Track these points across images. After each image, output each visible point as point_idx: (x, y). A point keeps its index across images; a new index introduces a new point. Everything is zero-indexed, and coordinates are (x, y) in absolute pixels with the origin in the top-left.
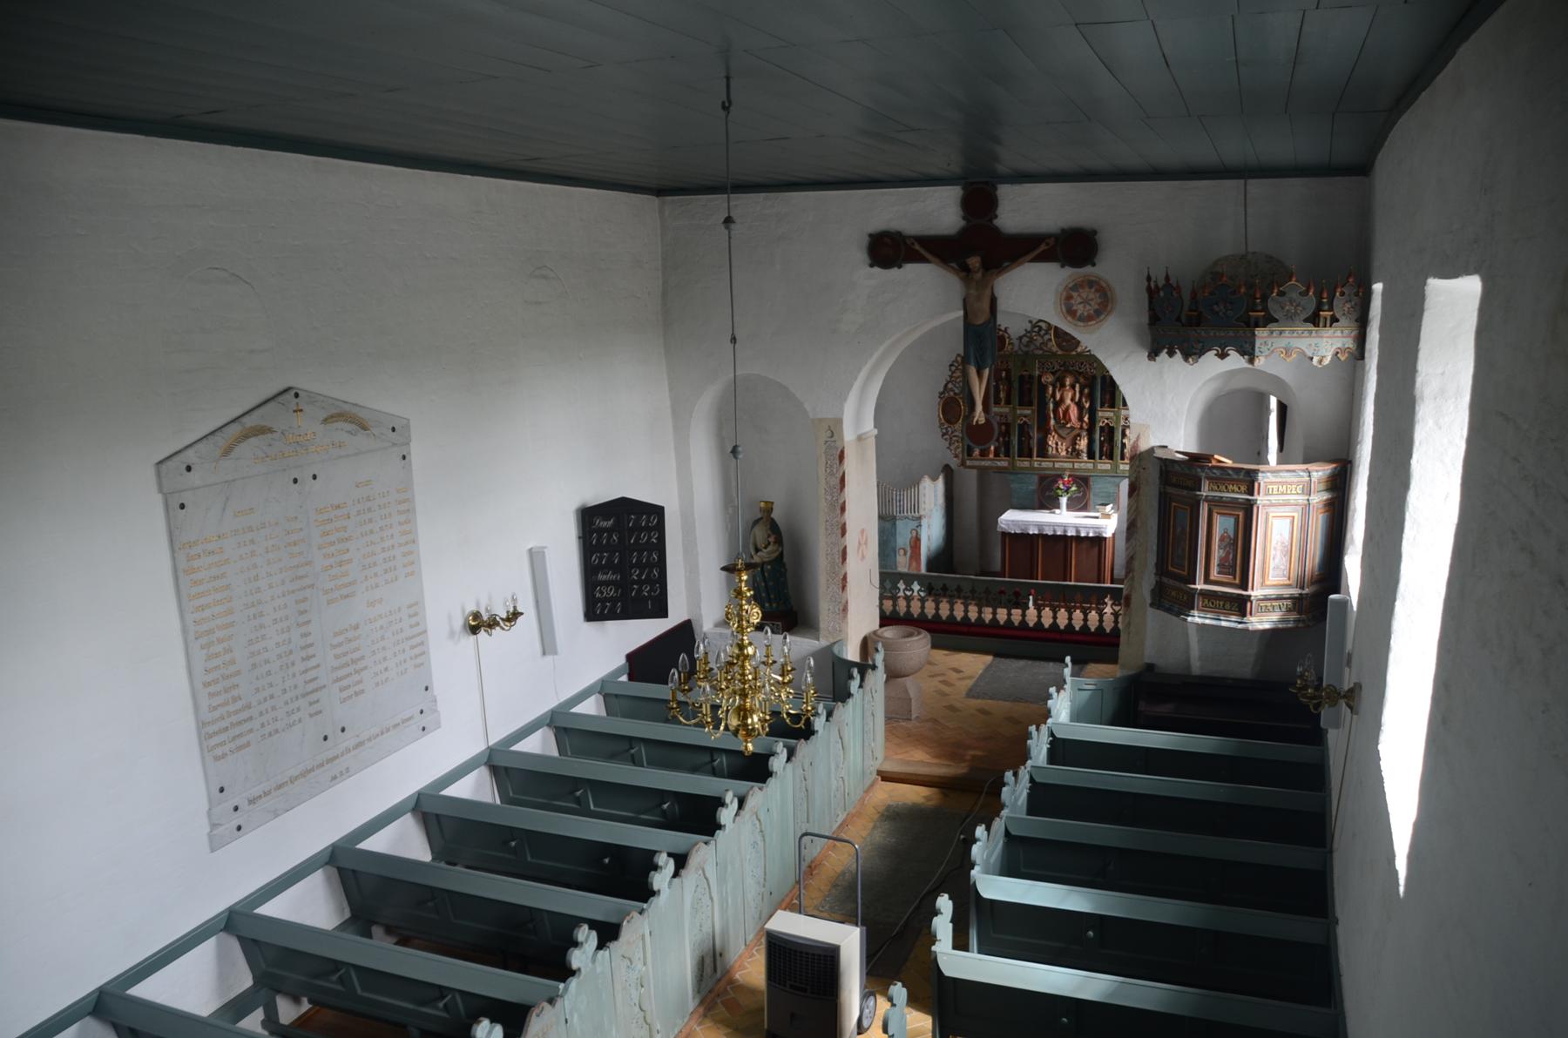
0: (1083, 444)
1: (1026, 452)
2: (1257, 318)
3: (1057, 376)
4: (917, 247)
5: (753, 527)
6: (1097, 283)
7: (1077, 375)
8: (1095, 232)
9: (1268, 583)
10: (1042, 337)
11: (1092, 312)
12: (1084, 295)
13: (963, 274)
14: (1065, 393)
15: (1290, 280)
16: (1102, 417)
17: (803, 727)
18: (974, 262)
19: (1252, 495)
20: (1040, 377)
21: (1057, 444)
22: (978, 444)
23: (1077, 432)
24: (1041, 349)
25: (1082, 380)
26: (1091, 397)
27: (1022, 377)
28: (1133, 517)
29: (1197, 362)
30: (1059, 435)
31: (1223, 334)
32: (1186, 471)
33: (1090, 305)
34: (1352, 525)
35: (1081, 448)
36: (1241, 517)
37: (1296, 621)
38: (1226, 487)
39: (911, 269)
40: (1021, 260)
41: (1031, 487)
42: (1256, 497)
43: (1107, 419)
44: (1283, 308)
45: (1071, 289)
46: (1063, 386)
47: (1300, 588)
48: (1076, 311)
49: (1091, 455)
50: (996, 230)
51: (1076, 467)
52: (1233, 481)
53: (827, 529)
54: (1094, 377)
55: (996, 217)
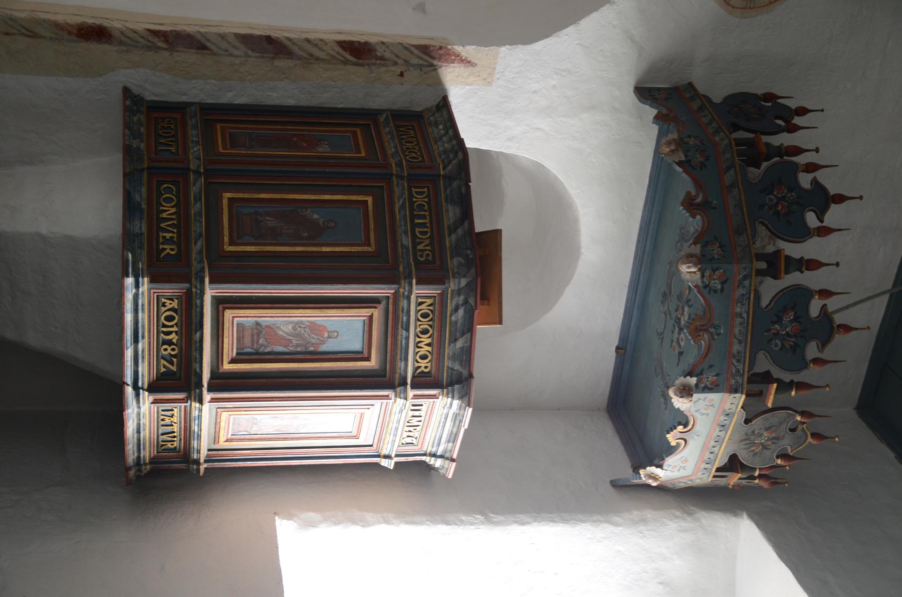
9: (224, 415)
28: (295, 49)
31: (736, 331)
32: (450, 241)
38: (424, 332)
42: (411, 393)
44: (767, 429)
47: (208, 456)
52: (438, 346)
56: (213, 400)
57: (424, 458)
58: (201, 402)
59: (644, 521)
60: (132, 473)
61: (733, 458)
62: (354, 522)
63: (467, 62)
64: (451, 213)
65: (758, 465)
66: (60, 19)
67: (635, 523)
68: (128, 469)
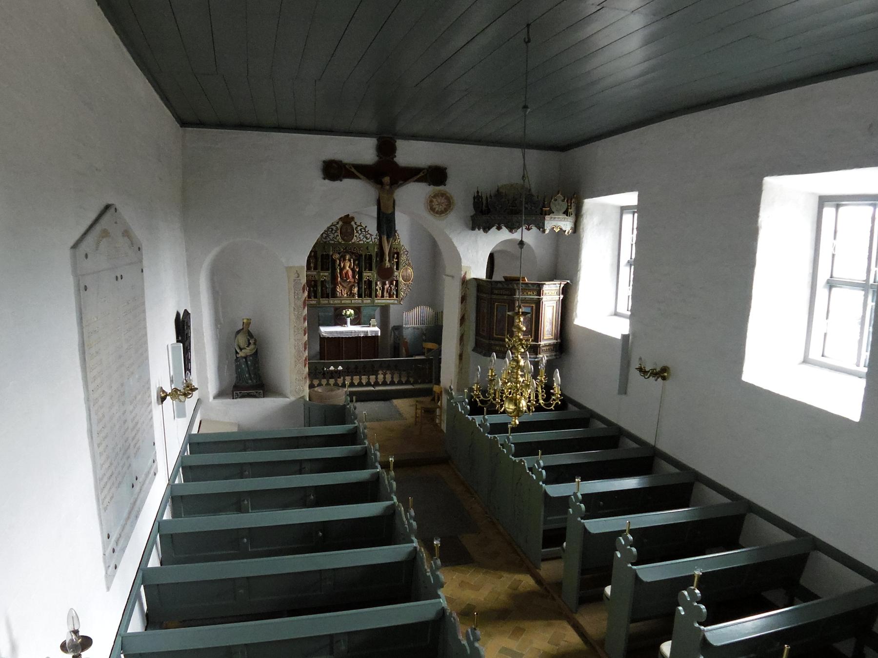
0: (356, 290)
1: (325, 295)
2: (546, 211)
3: (341, 254)
4: (353, 170)
5: (236, 337)
6: (445, 194)
7: (352, 253)
8: (446, 169)
9: (545, 338)
10: (334, 234)
11: (443, 209)
12: (439, 201)
13: (379, 186)
14: (346, 263)
15: (558, 194)
16: (366, 276)
17: (553, 409)
18: (387, 180)
19: (540, 296)
20: (332, 255)
21: (341, 291)
22: (387, 278)
23: (353, 284)
24: (333, 240)
25: (354, 257)
26: (359, 265)
27: (322, 255)
29: (516, 232)
30: (343, 286)
32: (506, 286)
33: (442, 206)
34: (576, 308)
35: (355, 292)
36: (534, 308)
37: (555, 355)
38: (527, 293)
39: (348, 183)
40: (410, 180)
41: (330, 314)
42: (542, 297)
43: (368, 277)
45: (432, 197)
46: (345, 260)
48: (435, 209)
49: (360, 296)
50: (396, 164)
51: (353, 302)
52: (530, 290)
53: (294, 331)
54: (361, 255)
55: (395, 156)
56: (540, 341)
57: (561, 288)
58: (540, 345)
59: (583, 228)
60: (558, 357)
61: (564, 213)
62: (577, 304)
63: (465, 274)
64: (499, 285)
65: (564, 205)
66: (458, 363)
67: (583, 231)
68: (557, 358)
